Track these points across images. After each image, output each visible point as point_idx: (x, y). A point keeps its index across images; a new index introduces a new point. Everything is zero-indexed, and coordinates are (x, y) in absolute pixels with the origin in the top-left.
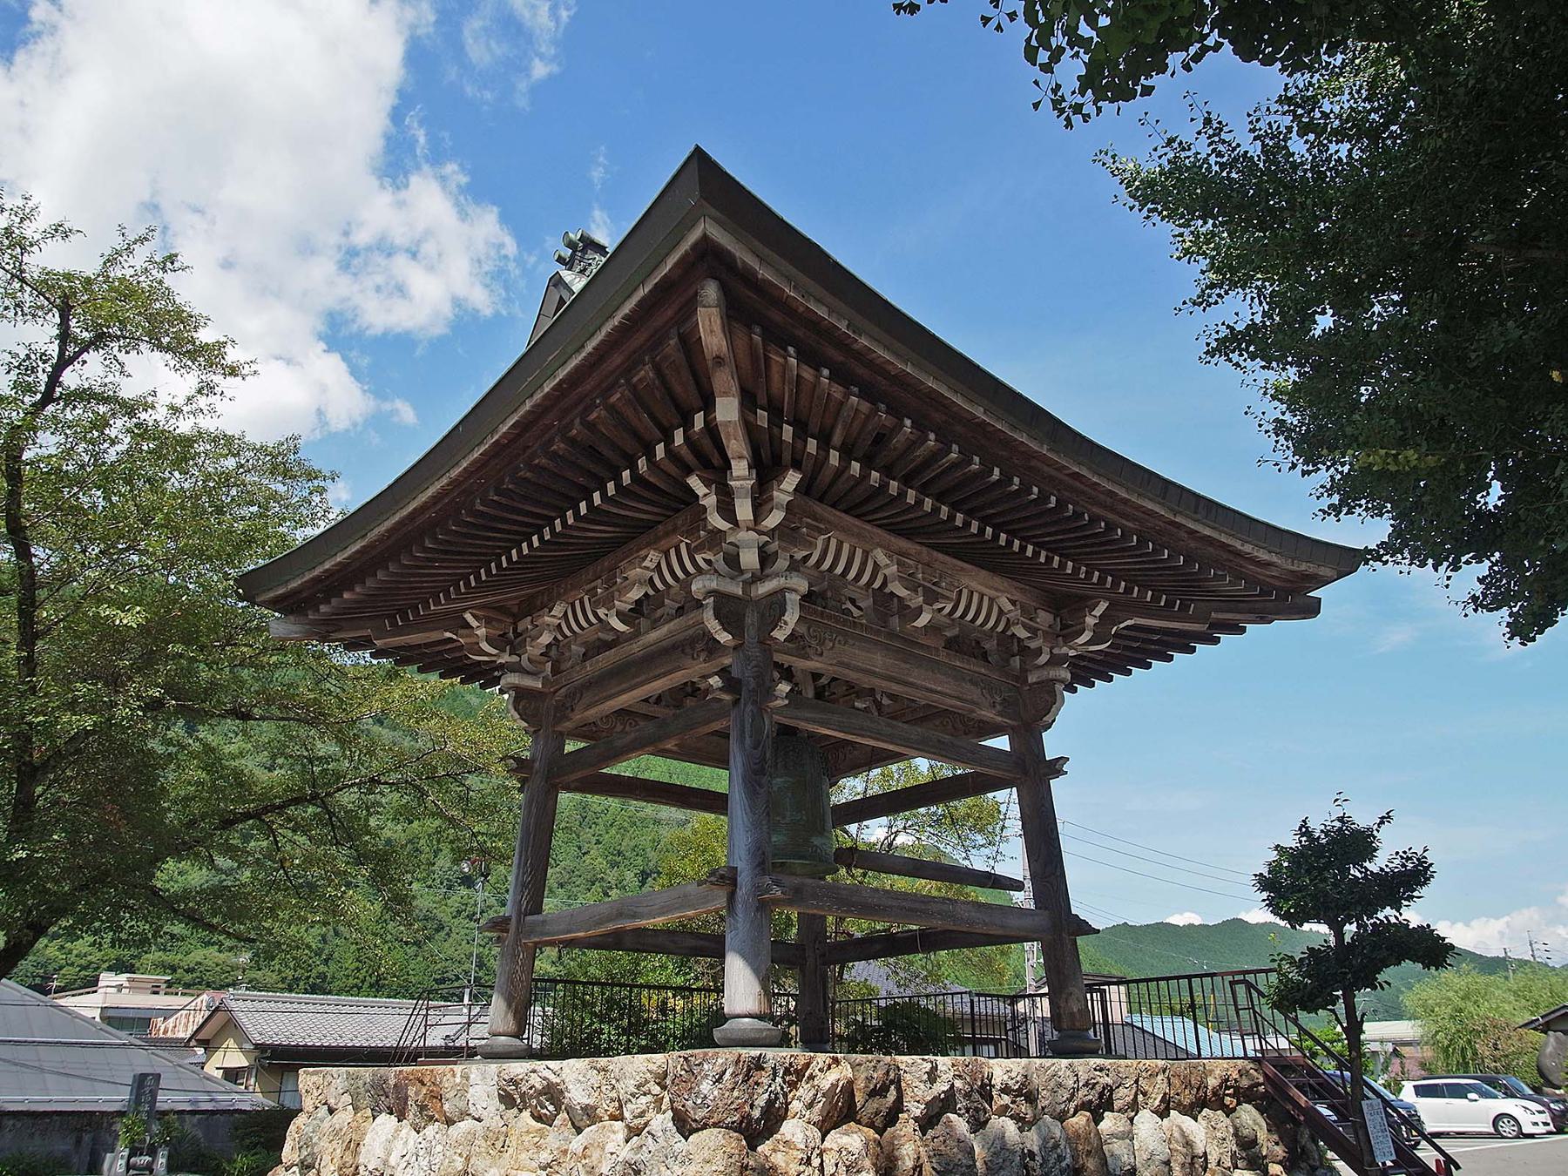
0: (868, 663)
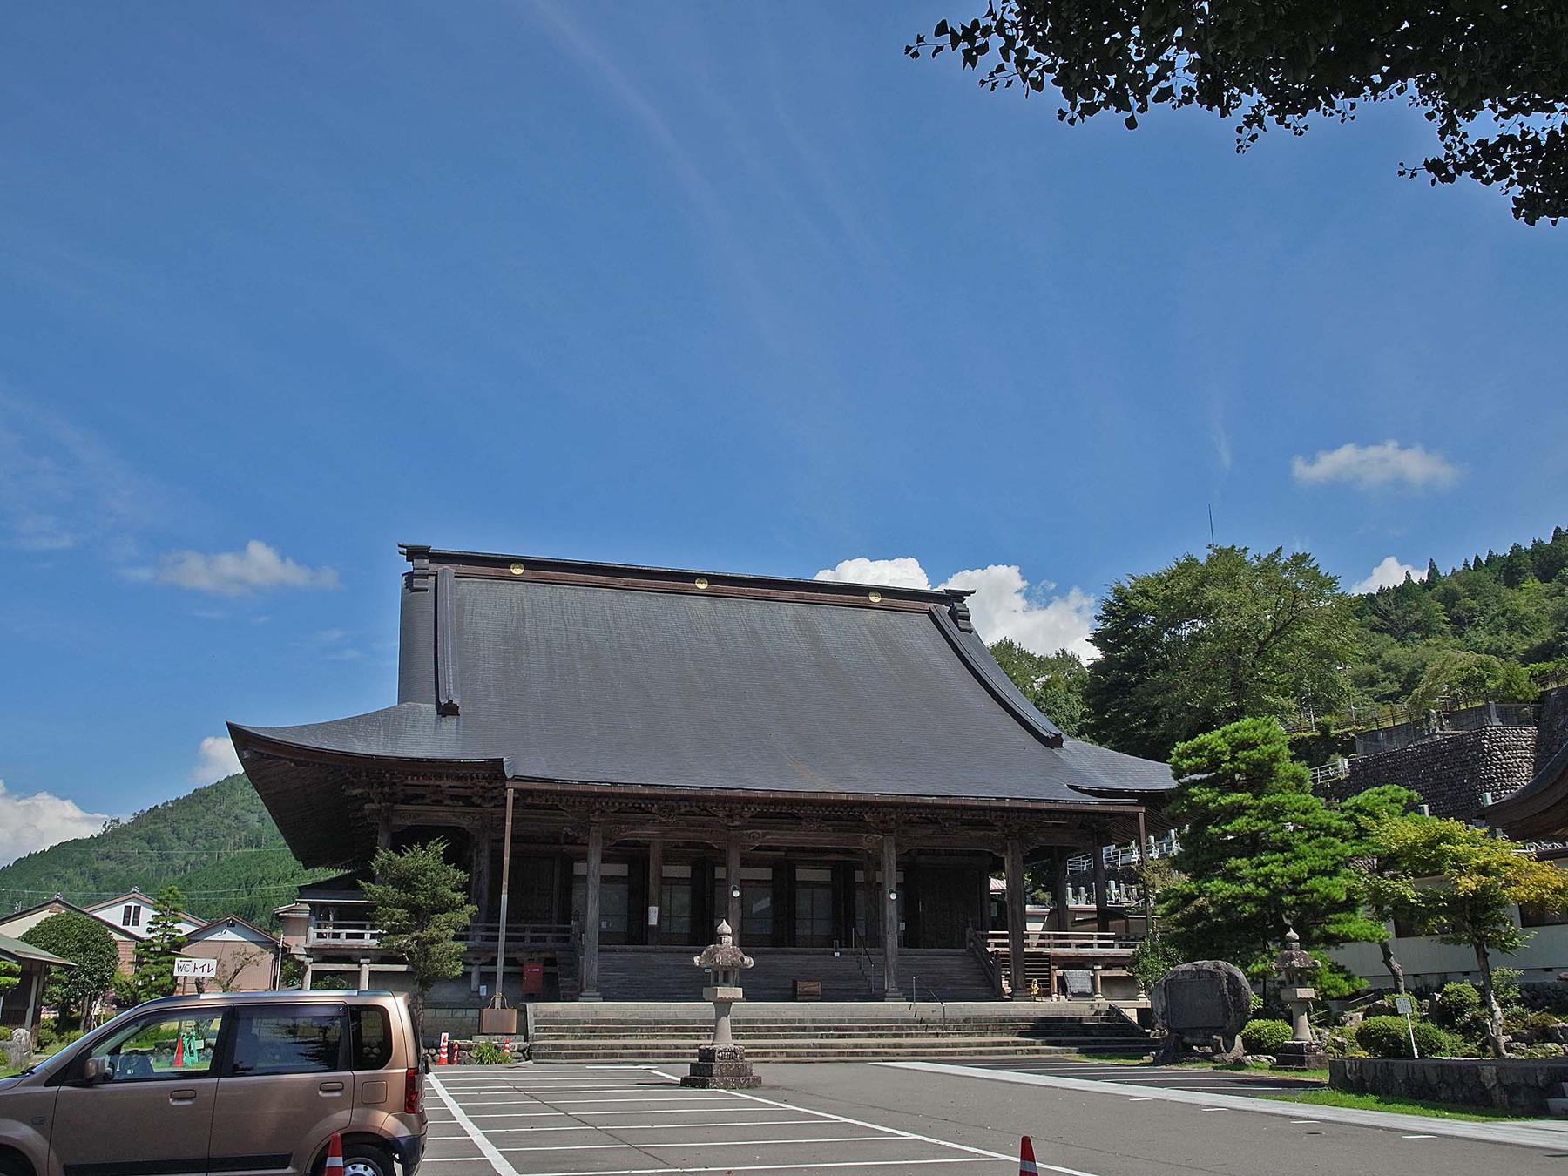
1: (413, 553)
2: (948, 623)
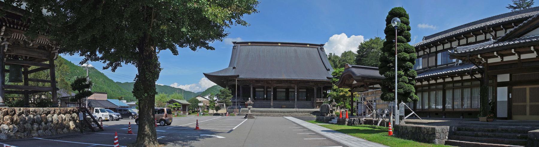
0: (22, 52)
1: (234, 43)
2: (319, 50)
